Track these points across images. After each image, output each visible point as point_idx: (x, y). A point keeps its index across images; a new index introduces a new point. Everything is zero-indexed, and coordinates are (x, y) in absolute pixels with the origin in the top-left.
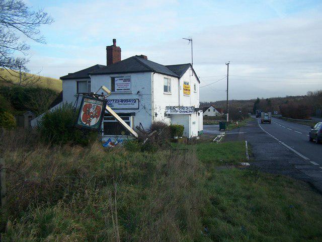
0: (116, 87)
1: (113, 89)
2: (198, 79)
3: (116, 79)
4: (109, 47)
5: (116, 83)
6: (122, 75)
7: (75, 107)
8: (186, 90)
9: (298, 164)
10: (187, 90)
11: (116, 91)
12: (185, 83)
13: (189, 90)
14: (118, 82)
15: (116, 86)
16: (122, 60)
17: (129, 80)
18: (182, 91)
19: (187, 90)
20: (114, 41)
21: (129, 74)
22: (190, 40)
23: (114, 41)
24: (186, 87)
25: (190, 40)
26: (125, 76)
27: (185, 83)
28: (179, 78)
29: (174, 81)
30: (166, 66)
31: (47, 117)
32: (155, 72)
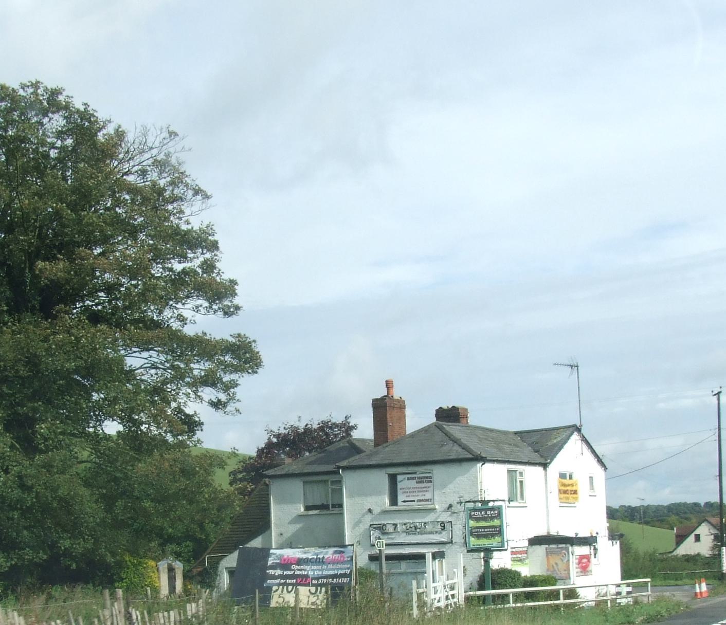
0: (401, 498)
1: (394, 501)
2: (600, 461)
3: (399, 478)
4: (377, 400)
5: (399, 486)
6: (411, 469)
7: (258, 499)
8: (565, 492)
9: (192, 610)
10: (568, 491)
11: (400, 503)
12: (562, 476)
13: (575, 492)
14: (404, 483)
15: (399, 492)
16: (407, 433)
17: (429, 480)
18: (555, 496)
19: (568, 491)
20: (389, 385)
21: (428, 468)
22: (572, 366)
23: (389, 385)
24: (564, 485)
25: (572, 366)
26: (421, 471)
27: (562, 476)
28: (545, 466)
29: (532, 474)
30: (516, 433)
31: (335, 598)
32: (484, 460)
